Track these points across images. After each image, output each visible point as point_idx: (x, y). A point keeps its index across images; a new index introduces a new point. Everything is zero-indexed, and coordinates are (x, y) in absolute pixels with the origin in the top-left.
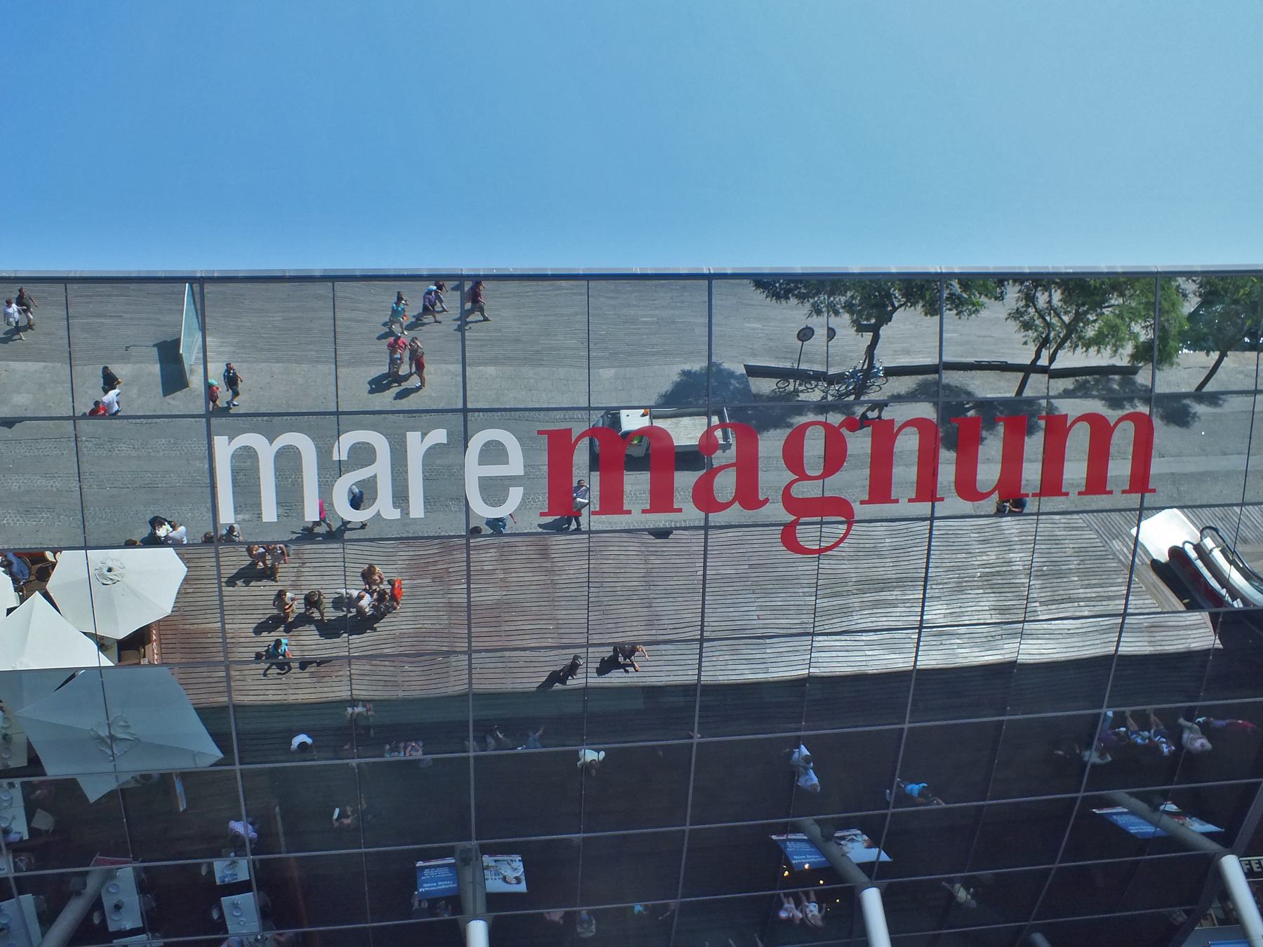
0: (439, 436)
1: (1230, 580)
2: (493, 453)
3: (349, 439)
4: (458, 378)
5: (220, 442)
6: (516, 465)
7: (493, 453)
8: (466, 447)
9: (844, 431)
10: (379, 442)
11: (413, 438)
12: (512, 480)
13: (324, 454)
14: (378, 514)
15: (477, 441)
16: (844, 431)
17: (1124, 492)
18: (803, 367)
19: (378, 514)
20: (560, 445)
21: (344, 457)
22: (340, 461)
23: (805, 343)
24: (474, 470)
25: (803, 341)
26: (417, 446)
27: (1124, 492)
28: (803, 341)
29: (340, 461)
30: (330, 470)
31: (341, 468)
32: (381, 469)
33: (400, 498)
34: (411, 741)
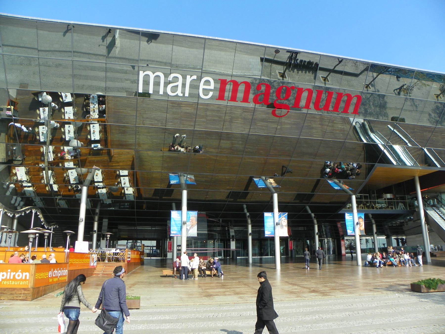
0: (195, 77)
1: (431, 208)
2: (207, 82)
3: (172, 75)
4: (229, 315)
5: (141, 72)
6: (212, 87)
7: (207, 82)
8: (201, 81)
9: (291, 89)
10: (180, 77)
11: (188, 77)
12: (211, 90)
13: (166, 76)
14: (154, 73)
15: (203, 80)
16: (291, 89)
17: (351, 113)
18: (275, 59)
19: (154, 73)
20: (223, 83)
21: (171, 80)
22: (173, 45)
23: (277, 54)
24: (202, 86)
25: (276, 53)
26: (189, 79)
27: (351, 113)
28: (276, 53)
29: (173, 45)
30: (166, 84)
31: (170, 82)
32: (180, 83)
33: (183, 93)
34: (176, 319)
